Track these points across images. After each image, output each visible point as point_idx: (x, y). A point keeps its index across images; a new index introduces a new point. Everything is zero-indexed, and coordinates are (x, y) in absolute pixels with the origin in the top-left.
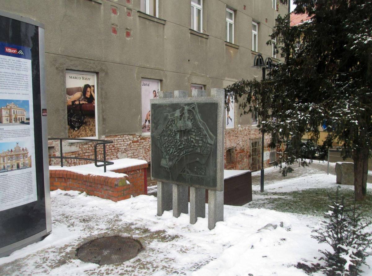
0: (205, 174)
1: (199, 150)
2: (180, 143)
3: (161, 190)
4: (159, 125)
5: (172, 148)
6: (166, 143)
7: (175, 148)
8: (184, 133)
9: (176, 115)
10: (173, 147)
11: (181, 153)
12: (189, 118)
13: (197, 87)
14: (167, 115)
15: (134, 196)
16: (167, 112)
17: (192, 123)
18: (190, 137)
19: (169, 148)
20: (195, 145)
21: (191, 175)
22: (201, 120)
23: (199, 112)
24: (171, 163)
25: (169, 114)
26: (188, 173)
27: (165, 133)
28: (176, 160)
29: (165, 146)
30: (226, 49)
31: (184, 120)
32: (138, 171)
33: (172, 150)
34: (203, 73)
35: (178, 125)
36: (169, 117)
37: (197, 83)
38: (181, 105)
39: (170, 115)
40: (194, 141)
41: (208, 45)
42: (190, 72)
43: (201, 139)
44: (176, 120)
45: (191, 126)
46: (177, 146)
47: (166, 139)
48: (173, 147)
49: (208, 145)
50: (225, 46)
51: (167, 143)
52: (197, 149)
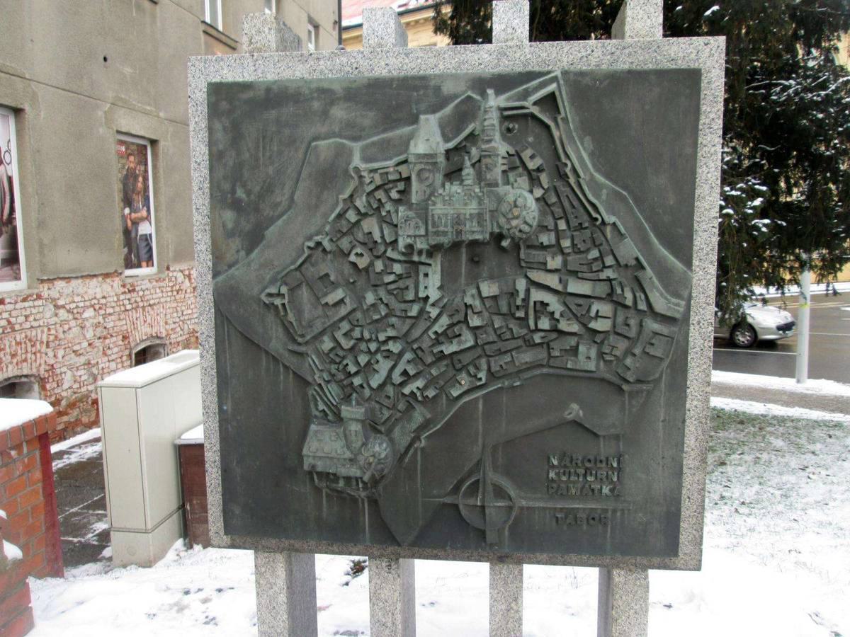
0: (616, 494)
1: (587, 358)
2: (445, 321)
3: (283, 598)
4: (272, 220)
5: (388, 355)
6: (335, 326)
7: (408, 356)
8: (475, 261)
9: (419, 147)
10: (395, 347)
11: (455, 382)
12: (515, 163)
13: (133, 144)
14: (342, 153)
15: (30, 602)
16: (334, 135)
17: (539, 193)
18: (521, 285)
19: (363, 359)
20: (563, 326)
21: (524, 503)
22: (600, 178)
23: (586, 128)
24: (380, 448)
25: (356, 147)
26: (500, 493)
27: (326, 267)
28: (414, 426)
29: (327, 344)
30: (206, 43)
31: (480, 177)
32: (13, 453)
33: (384, 366)
34: (149, 105)
35: (438, 209)
36: (356, 161)
37: (133, 132)
38: (448, 88)
39: (364, 149)
40: (555, 305)
41: (159, 24)
42: (110, 95)
43: (602, 290)
44: (420, 180)
45: (536, 214)
46: (426, 344)
47: (342, 301)
48: (395, 347)
49: (652, 325)
50: (202, 33)
51: (345, 326)
52: (574, 351)
